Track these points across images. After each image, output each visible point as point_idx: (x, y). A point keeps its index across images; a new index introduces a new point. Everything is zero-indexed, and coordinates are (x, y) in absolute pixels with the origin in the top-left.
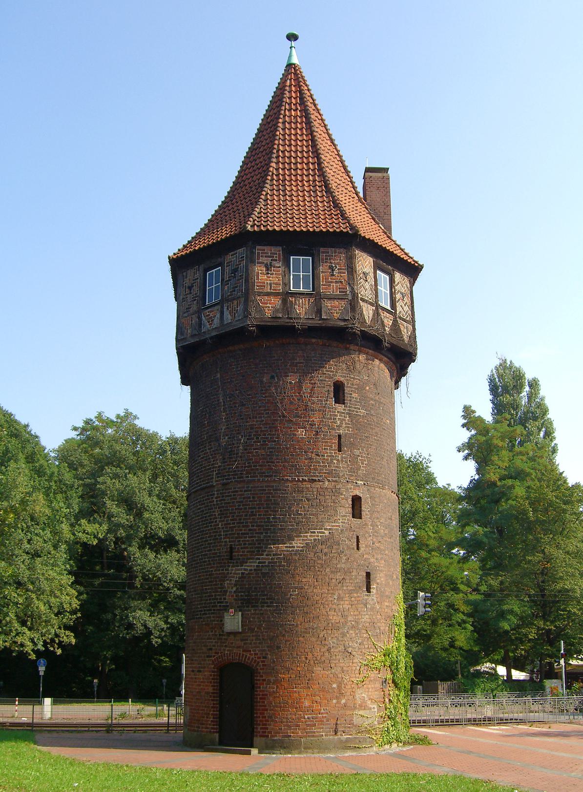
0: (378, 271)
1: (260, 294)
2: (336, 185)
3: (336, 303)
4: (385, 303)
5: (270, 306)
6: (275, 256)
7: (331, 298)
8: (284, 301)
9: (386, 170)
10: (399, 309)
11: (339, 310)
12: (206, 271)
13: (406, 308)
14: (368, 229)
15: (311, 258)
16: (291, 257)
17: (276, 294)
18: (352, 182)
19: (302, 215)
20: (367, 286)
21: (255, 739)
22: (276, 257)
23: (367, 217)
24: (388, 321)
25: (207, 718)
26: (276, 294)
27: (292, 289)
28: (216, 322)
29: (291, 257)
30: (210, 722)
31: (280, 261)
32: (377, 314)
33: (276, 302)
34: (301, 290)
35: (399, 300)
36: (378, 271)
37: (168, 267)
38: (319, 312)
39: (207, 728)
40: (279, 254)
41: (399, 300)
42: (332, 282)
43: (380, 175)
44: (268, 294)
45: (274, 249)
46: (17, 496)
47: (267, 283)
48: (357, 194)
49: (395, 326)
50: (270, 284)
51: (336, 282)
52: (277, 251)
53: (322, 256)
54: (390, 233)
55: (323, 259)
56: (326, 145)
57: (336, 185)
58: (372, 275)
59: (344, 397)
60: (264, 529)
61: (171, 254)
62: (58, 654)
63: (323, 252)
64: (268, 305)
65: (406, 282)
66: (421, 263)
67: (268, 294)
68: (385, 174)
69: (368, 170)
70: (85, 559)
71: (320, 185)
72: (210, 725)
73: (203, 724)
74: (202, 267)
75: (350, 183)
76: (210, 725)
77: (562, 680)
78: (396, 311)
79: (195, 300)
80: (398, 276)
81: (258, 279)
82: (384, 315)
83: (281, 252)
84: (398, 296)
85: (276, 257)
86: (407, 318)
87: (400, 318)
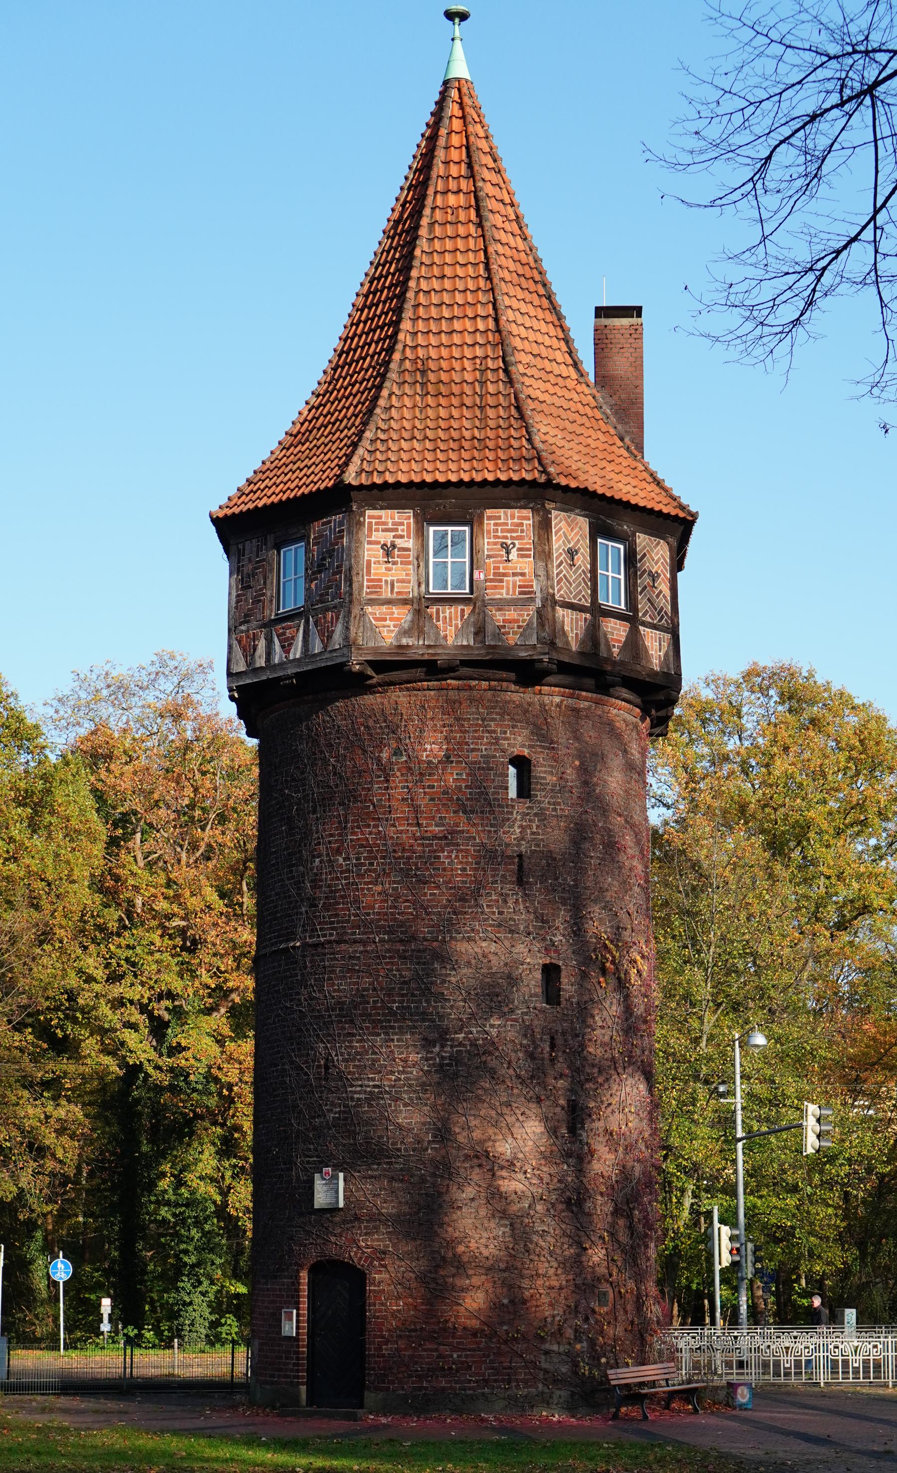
0: (599, 540)
1: (372, 602)
5: (392, 623)
6: (400, 528)
8: (418, 613)
9: (637, 311)
11: (519, 627)
15: (467, 529)
17: (405, 602)
18: (567, 341)
19: (454, 440)
21: (366, 1393)
25: (287, 1358)
26: (405, 602)
27: (431, 590)
28: (297, 652)
30: (291, 1366)
31: (409, 537)
34: (449, 591)
36: (599, 540)
39: (286, 1376)
40: (409, 525)
42: (505, 575)
43: (625, 322)
44: (389, 602)
47: (386, 581)
51: (514, 574)
59: (530, 783)
60: (382, 1028)
61: (215, 508)
63: (489, 518)
64: (388, 622)
66: (693, 509)
67: (389, 602)
68: (634, 320)
69: (601, 312)
70: (547, 1422)
71: (495, 367)
73: (280, 1370)
75: (562, 343)
80: (642, 540)
81: (369, 573)
83: (412, 520)
86: (660, 620)
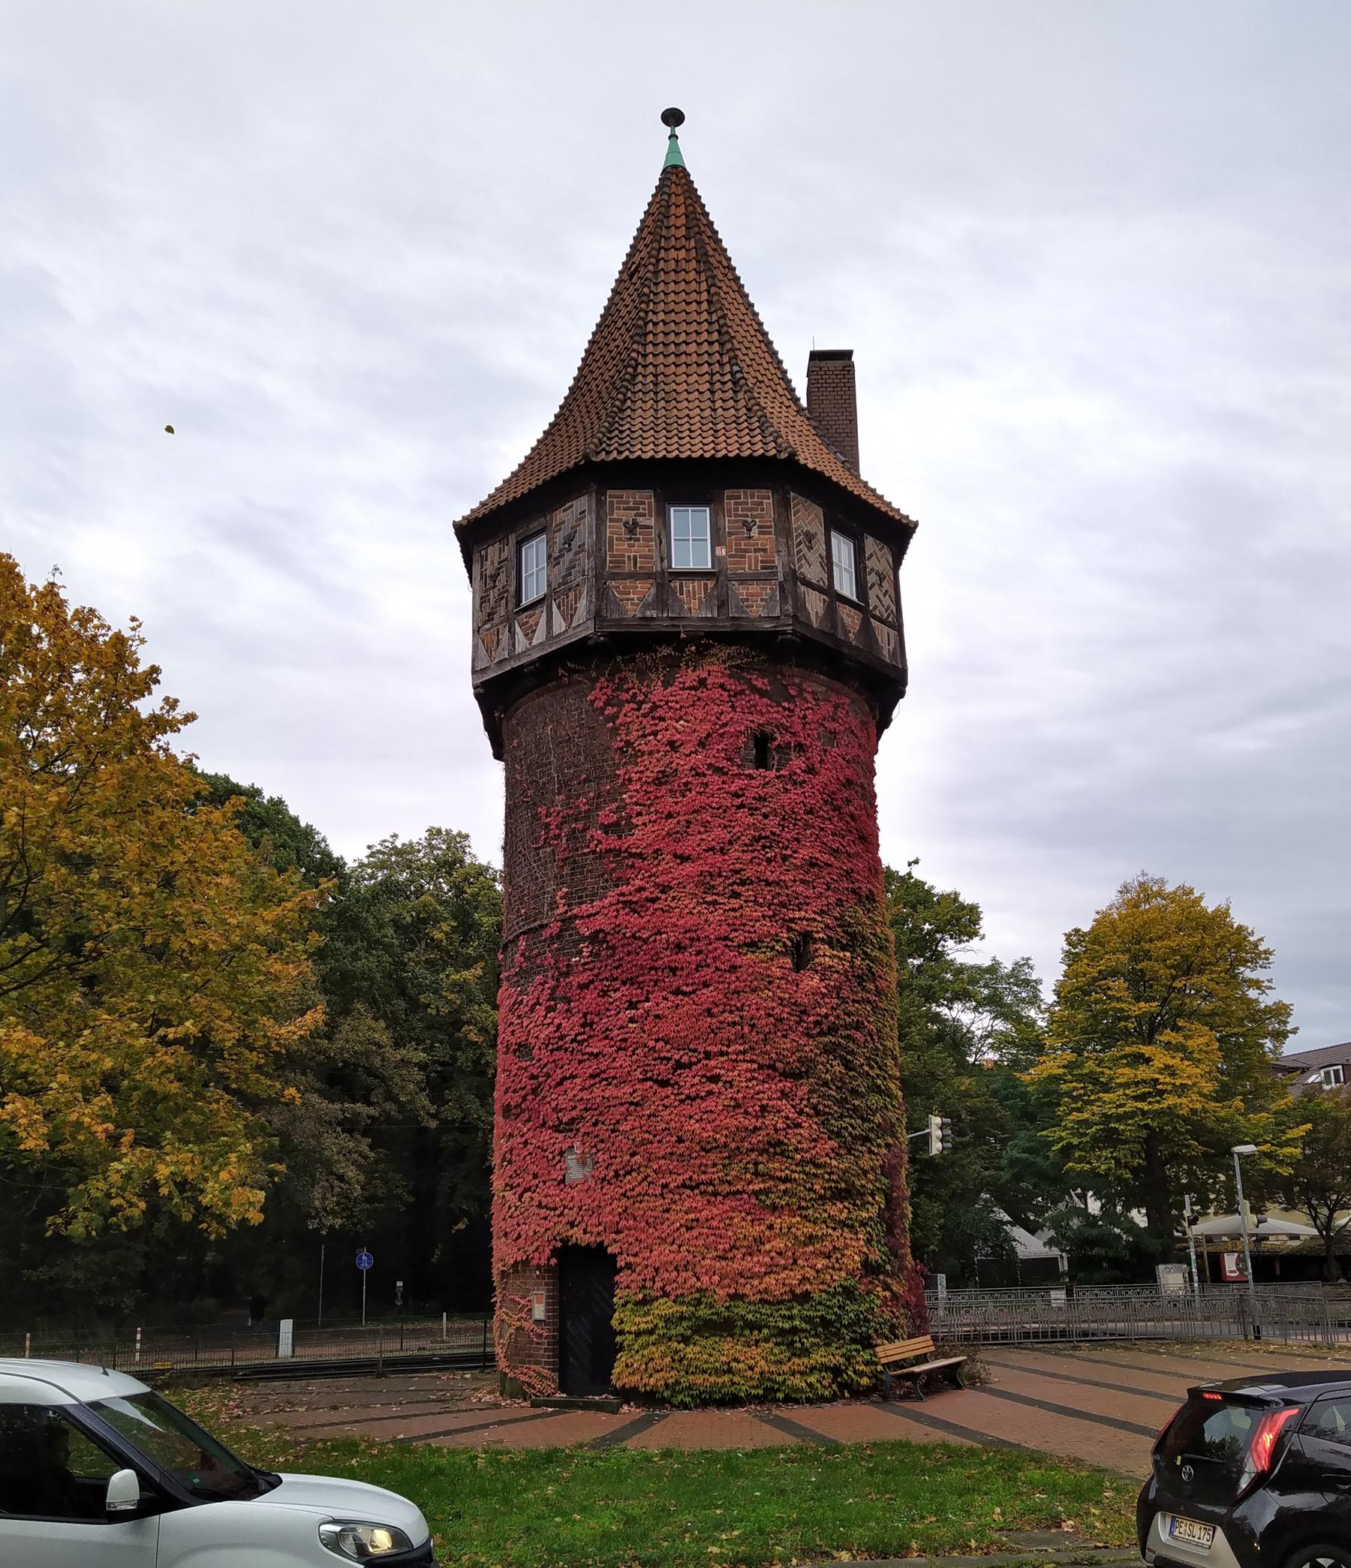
2: (755, 381)
3: (754, 588)
4: (846, 585)
7: (744, 580)
8: (661, 587)
9: (847, 355)
10: (873, 602)
12: (519, 544)
13: (887, 601)
14: (813, 455)
16: (672, 509)
17: (648, 576)
20: (812, 556)
22: (644, 509)
23: (814, 441)
24: (850, 619)
26: (648, 576)
29: (672, 509)
32: (831, 611)
33: (645, 590)
35: (873, 585)
37: (455, 546)
38: (723, 605)
40: (650, 503)
41: (873, 585)
42: (746, 551)
45: (639, 495)
46: (159, 737)
48: (797, 400)
49: (866, 629)
50: (635, 558)
51: (756, 551)
52: (645, 498)
53: (729, 504)
54: (857, 470)
55: (729, 510)
56: (738, 312)
57: (755, 381)
58: (821, 537)
61: (459, 519)
62: (256, 1217)
63: (729, 498)
64: (631, 596)
65: (887, 555)
69: (815, 356)
72: (543, 1356)
74: (512, 539)
76: (543, 1356)
77: (1189, 1264)
78: (868, 604)
79: (502, 598)
80: (870, 544)
81: (611, 549)
82: (845, 612)
84: (872, 578)
85: (644, 509)
87: (874, 617)
